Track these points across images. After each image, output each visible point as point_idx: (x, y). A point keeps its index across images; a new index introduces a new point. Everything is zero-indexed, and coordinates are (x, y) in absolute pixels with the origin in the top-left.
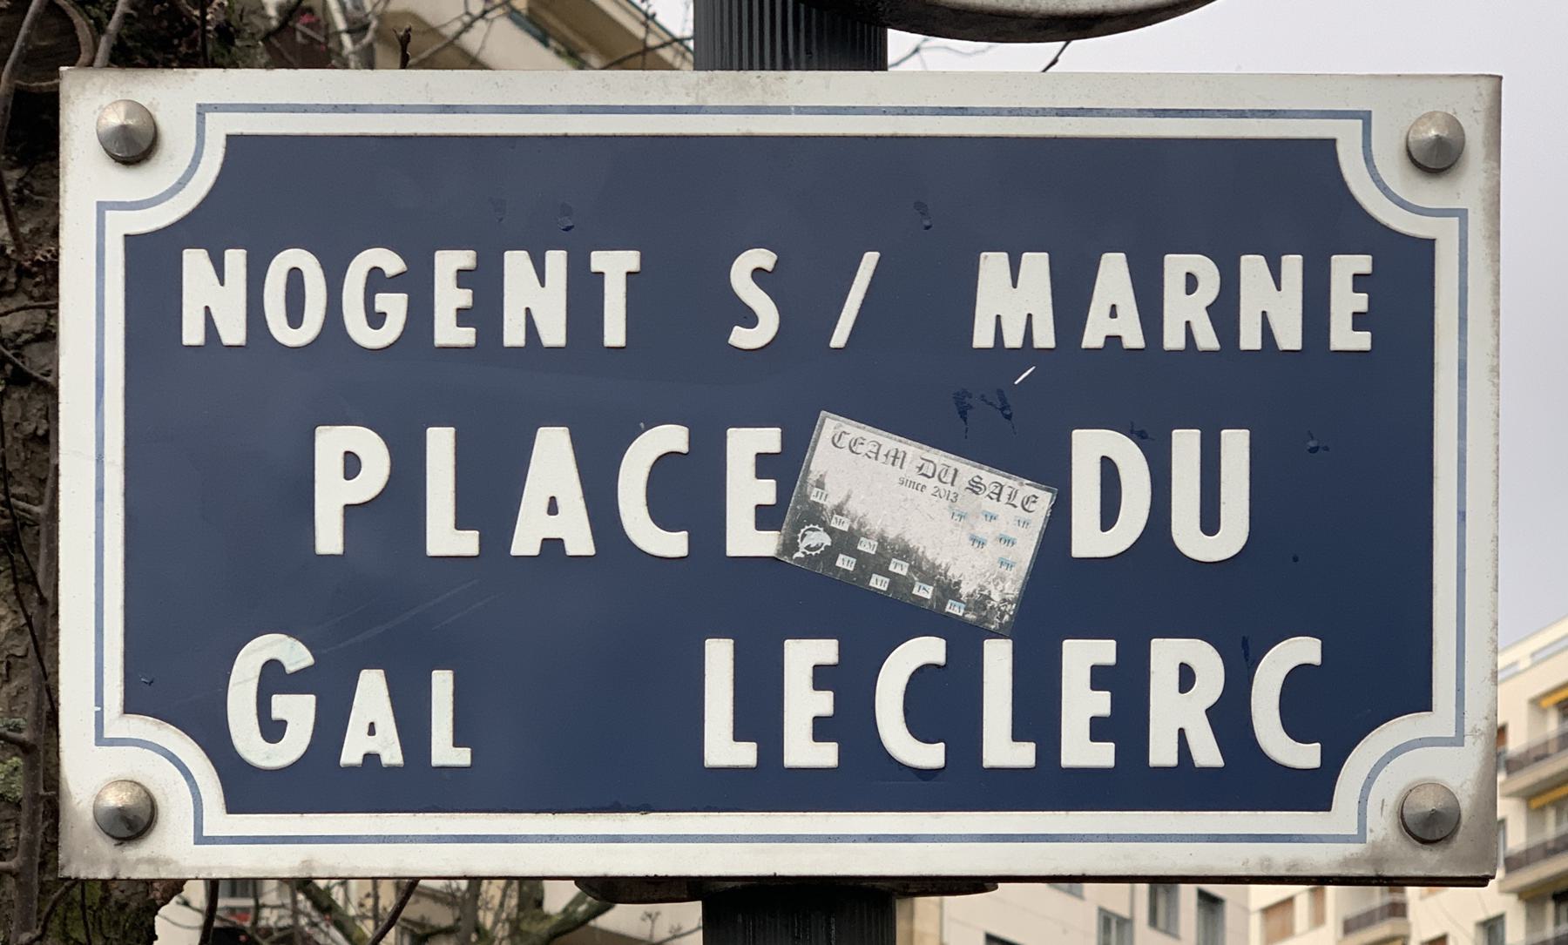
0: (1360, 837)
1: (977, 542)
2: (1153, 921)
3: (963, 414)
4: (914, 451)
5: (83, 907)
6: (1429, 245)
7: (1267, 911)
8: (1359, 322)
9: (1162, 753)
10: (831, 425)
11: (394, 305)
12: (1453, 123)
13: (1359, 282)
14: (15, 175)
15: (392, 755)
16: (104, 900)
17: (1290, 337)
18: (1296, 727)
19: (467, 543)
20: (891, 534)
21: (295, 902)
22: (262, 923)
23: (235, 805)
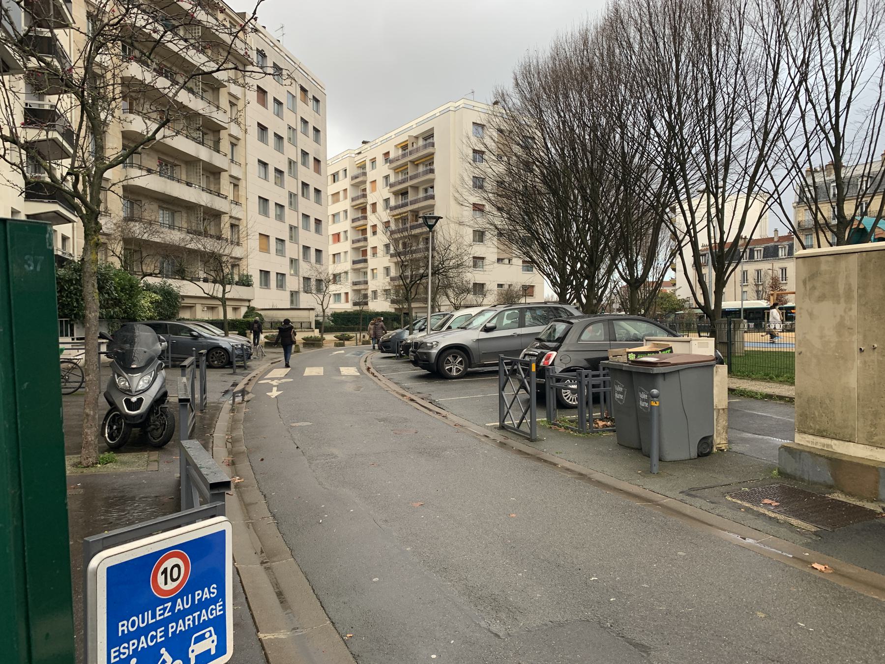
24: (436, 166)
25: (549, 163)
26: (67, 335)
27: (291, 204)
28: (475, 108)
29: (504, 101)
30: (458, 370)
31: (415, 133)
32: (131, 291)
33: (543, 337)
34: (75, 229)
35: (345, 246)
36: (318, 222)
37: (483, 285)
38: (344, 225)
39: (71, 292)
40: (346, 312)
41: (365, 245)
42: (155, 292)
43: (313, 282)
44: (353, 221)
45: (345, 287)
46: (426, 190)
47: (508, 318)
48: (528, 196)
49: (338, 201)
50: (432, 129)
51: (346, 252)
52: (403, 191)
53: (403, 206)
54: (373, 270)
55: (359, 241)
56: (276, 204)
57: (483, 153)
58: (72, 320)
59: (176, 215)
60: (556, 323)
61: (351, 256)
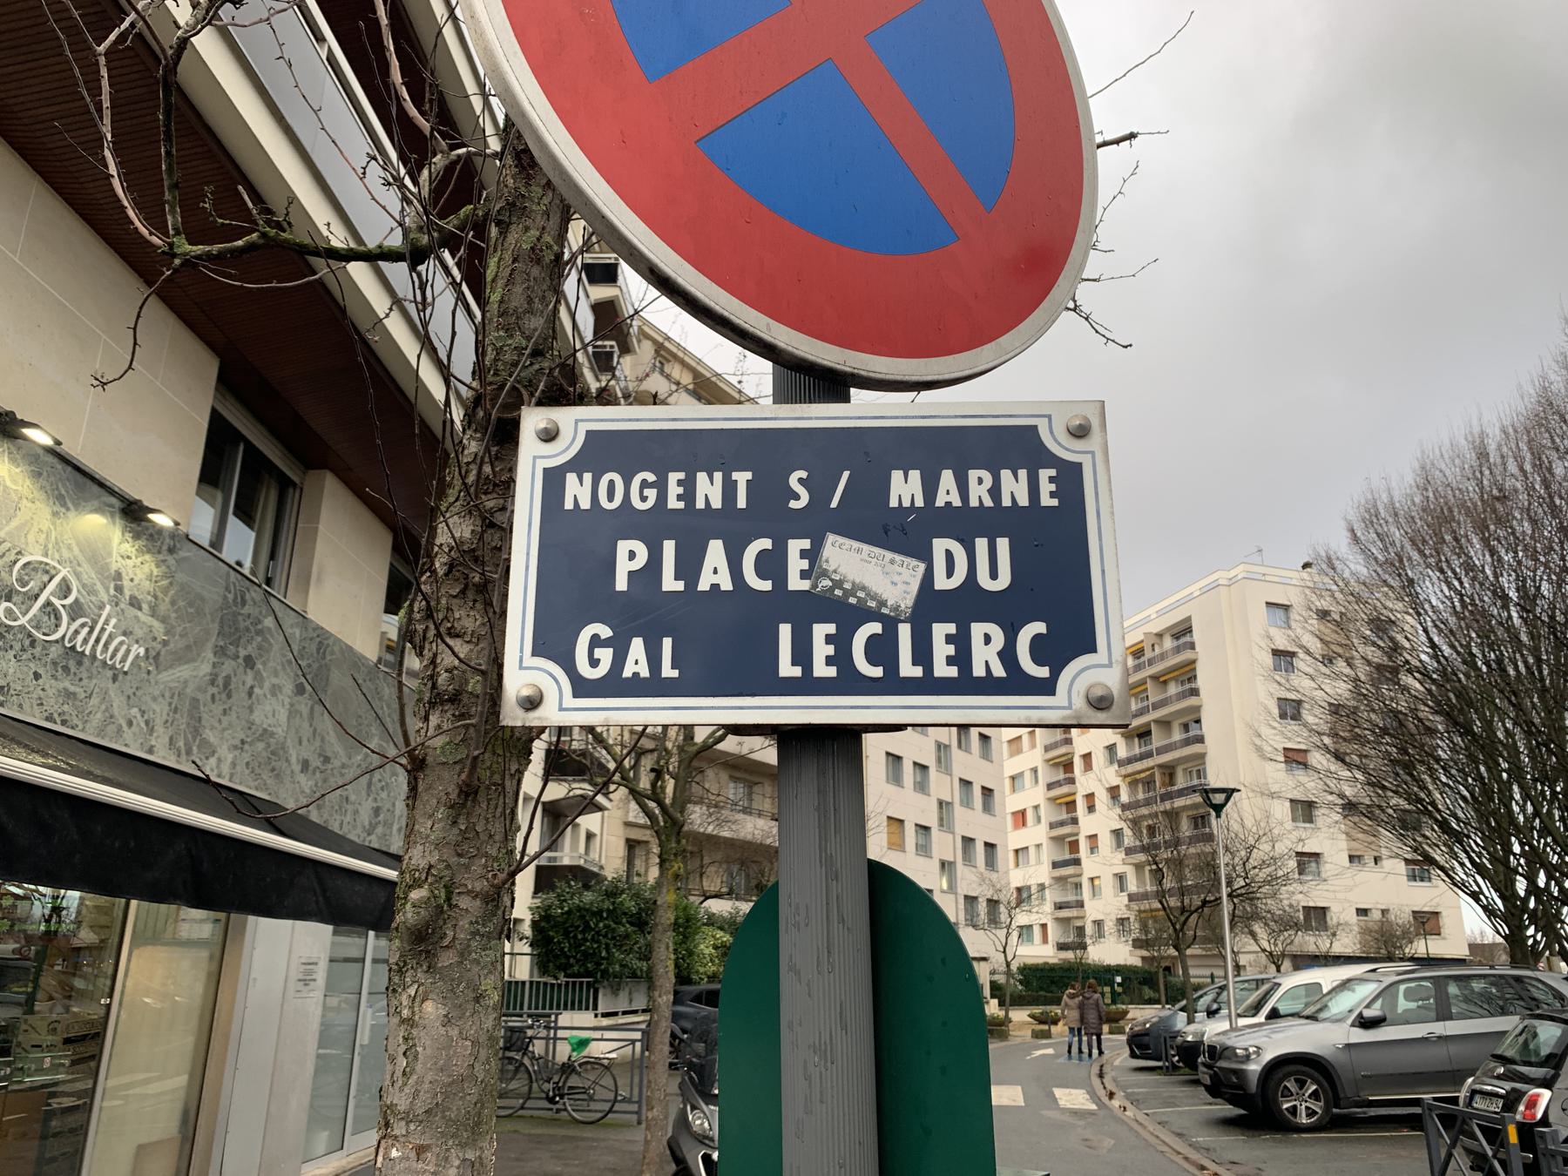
0: (1070, 707)
1: (894, 584)
2: (960, 746)
3: (886, 533)
4: (866, 548)
5: (503, 740)
6: (1080, 465)
7: (1010, 742)
8: (1052, 495)
9: (979, 671)
10: (831, 538)
11: (652, 494)
12: (1086, 418)
13: (1051, 480)
14: (495, 449)
15: (645, 672)
16: (511, 737)
17: (1023, 501)
18: (1037, 659)
19: (680, 586)
20: (857, 581)
21: (587, 738)
22: (573, 747)
23: (577, 694)
24: (1201, 682)
25: (1444, 673)
26: (587, 1009)
27: (939, 760)
28: (1268, 578)
29: (1333, 569)
30: (1311, 1113)
31: (1156, 627)
32: (687, 928)
33: (1510, 1053)
34: (606, 820)
35: (1036, 834)
36: (987, 792)
37: (1324, 910)
38: (1033, 796)
39: (598, 933)
40: (1046, 963)
41: (1075, 831)
42: (721, 928)
43: (982, 907)
44: (1050, 786)
45: (1041, 913)
46: (1186, 727)
47: (1409, 995)
48: (1398, 727)
49: (1019, 751)
50: (1189, 619)
51: (1038, 846)
52: (1141, 730)
53: (1142, 757)
54: (1092, 879)
55: (1062, 824)
56: (915, 764)
57: (1293, 654)
58: (596, 981)
59: (756, 789)
60: (1536, 1022)
61: (1048, 854)
